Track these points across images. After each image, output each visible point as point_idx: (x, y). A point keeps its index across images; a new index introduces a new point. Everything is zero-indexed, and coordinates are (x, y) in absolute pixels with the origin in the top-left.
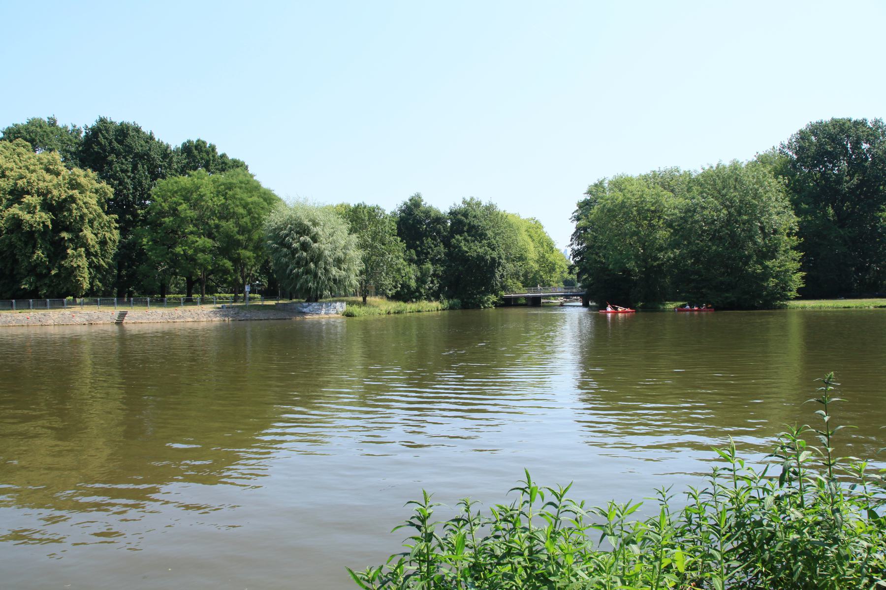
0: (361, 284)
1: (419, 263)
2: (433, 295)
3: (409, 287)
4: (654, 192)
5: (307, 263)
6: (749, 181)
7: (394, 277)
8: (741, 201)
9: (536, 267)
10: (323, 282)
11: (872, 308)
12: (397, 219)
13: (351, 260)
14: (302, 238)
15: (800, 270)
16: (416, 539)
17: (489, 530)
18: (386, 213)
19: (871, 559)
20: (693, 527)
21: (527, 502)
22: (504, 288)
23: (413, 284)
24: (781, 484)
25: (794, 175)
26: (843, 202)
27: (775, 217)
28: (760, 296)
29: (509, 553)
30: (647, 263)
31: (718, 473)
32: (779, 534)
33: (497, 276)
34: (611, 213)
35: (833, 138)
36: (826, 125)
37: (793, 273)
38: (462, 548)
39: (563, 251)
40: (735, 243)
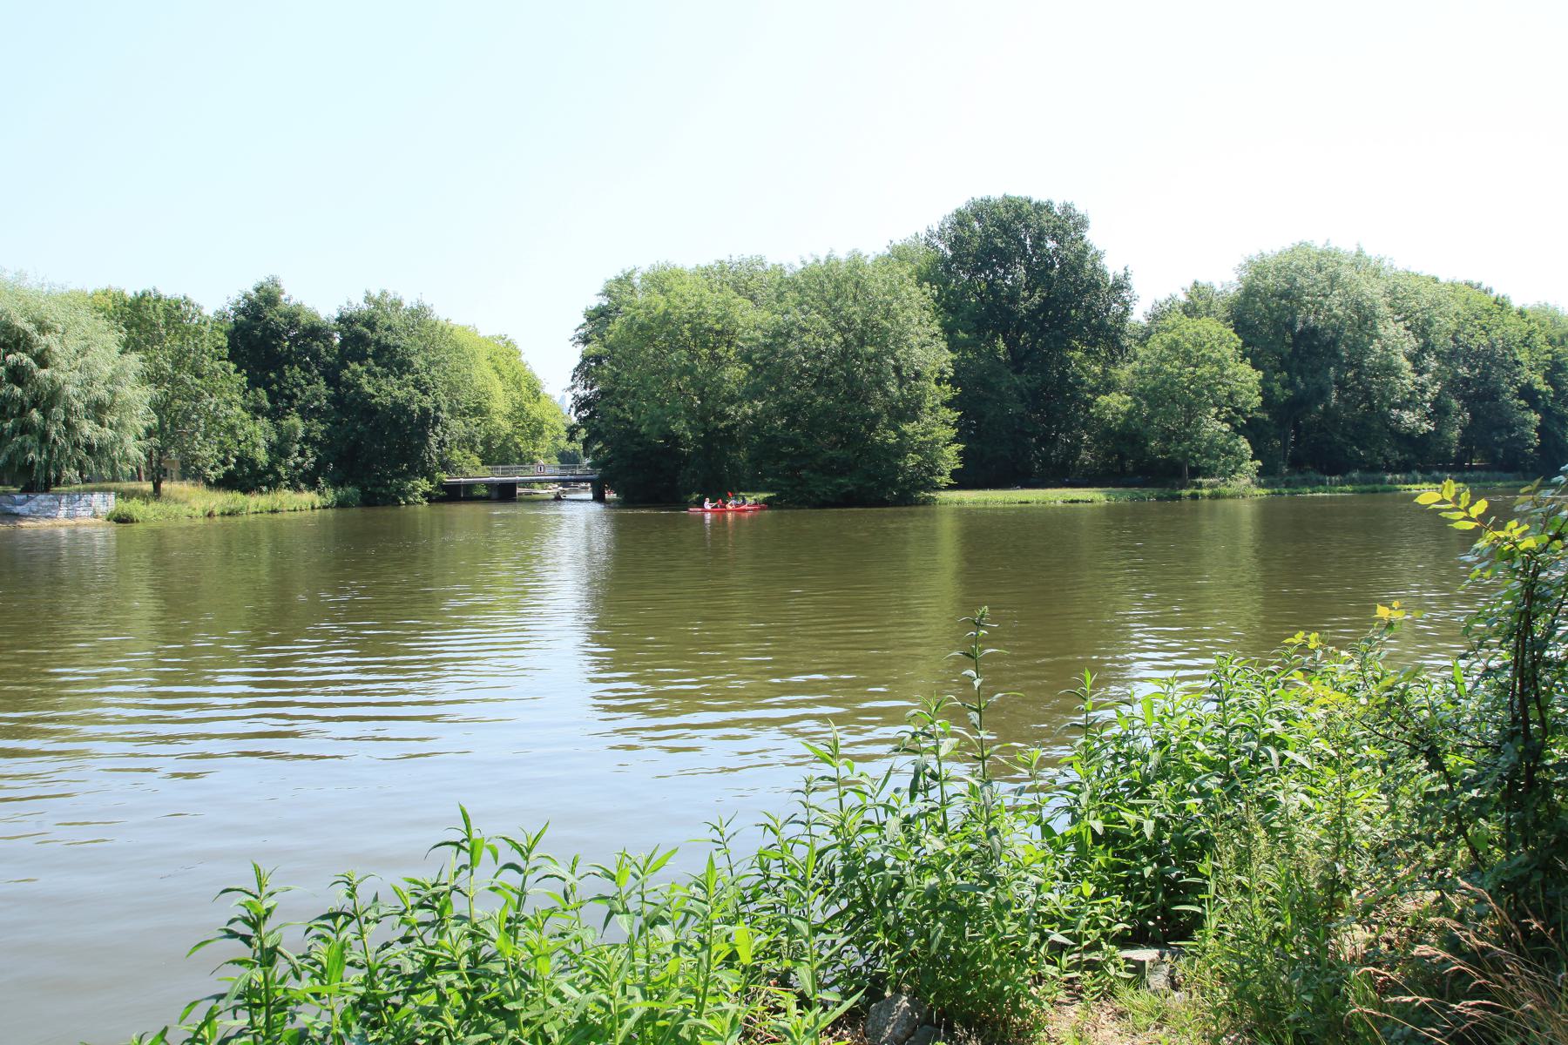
0: (149, 456)
1: (275, 415)
2: (303, 478)
3: (252, 463)
4: (721, 297)
5: (23, 411)
6: (876, 287)
7: (221, 442)
8: (864, 322)
9: (507, 427)
10: (62, 451)
11: (1059, 503)
12: (228, 325)
13: (126, 406)
14: (10, 357)
15: (954, 441)
16: (241, 963)
17: (391, 930)
18: (205, 312)
19: (1044, 902)
20: (773, 883)
21: (465, 867)
22: (446, 466)
23: (262, 456)
24: (912, 796)
25: (947, 284)
26: (1019, 331)
27: (917, 351)
28: (894, 483)
29: (431, 967)
30: (707, 423)
31: (813, 785)
32: (908, 880)
33: (433, 442)
34: (644, 332)
35: (1004, 228)
36: (996, 206)
37: (945, 446)
38: (340, 969)
39: (557, 399)
40: (856, 394)
